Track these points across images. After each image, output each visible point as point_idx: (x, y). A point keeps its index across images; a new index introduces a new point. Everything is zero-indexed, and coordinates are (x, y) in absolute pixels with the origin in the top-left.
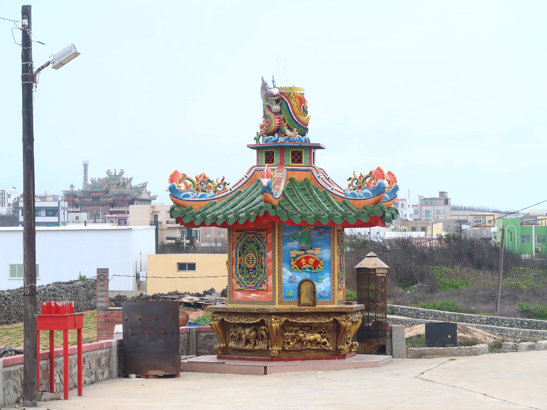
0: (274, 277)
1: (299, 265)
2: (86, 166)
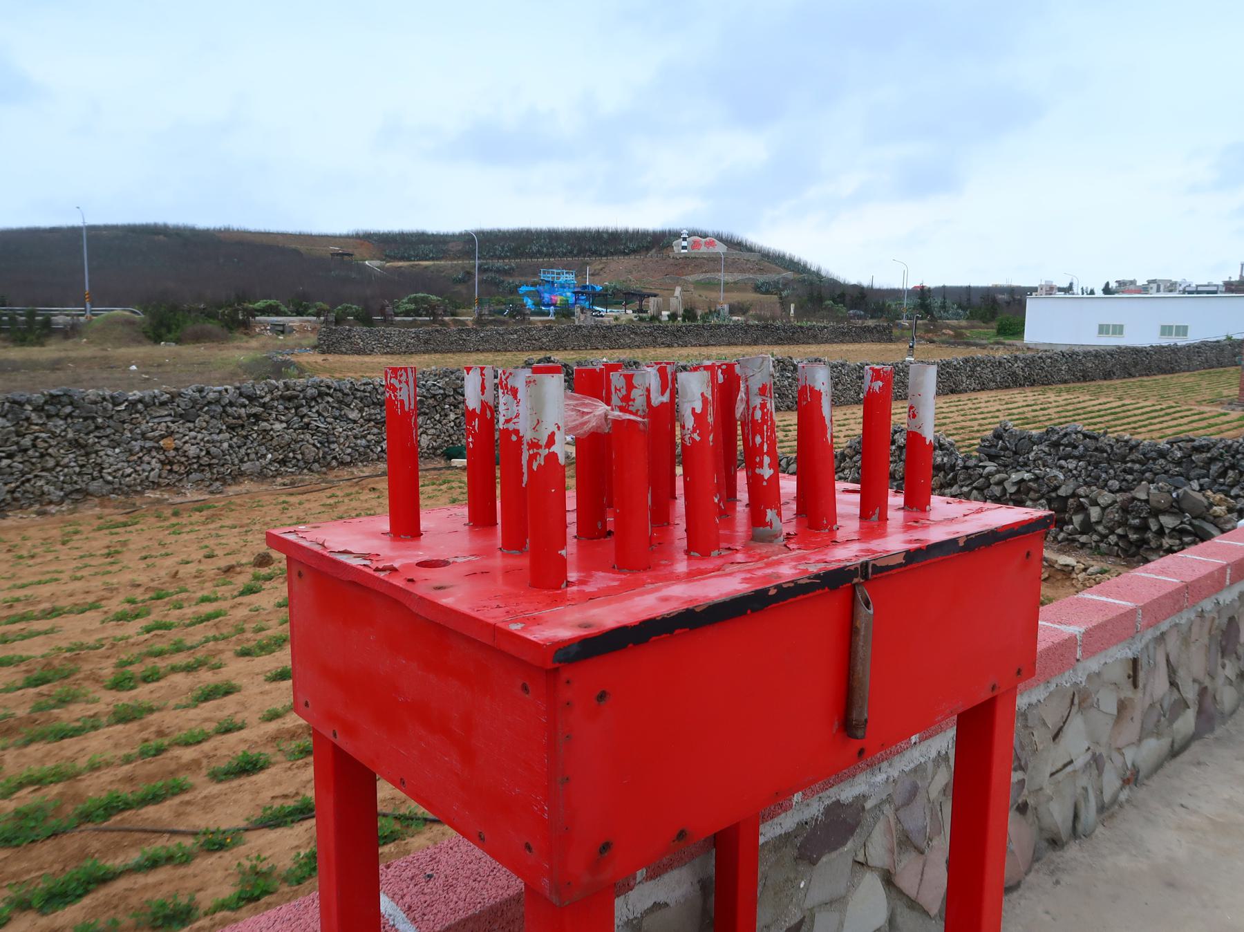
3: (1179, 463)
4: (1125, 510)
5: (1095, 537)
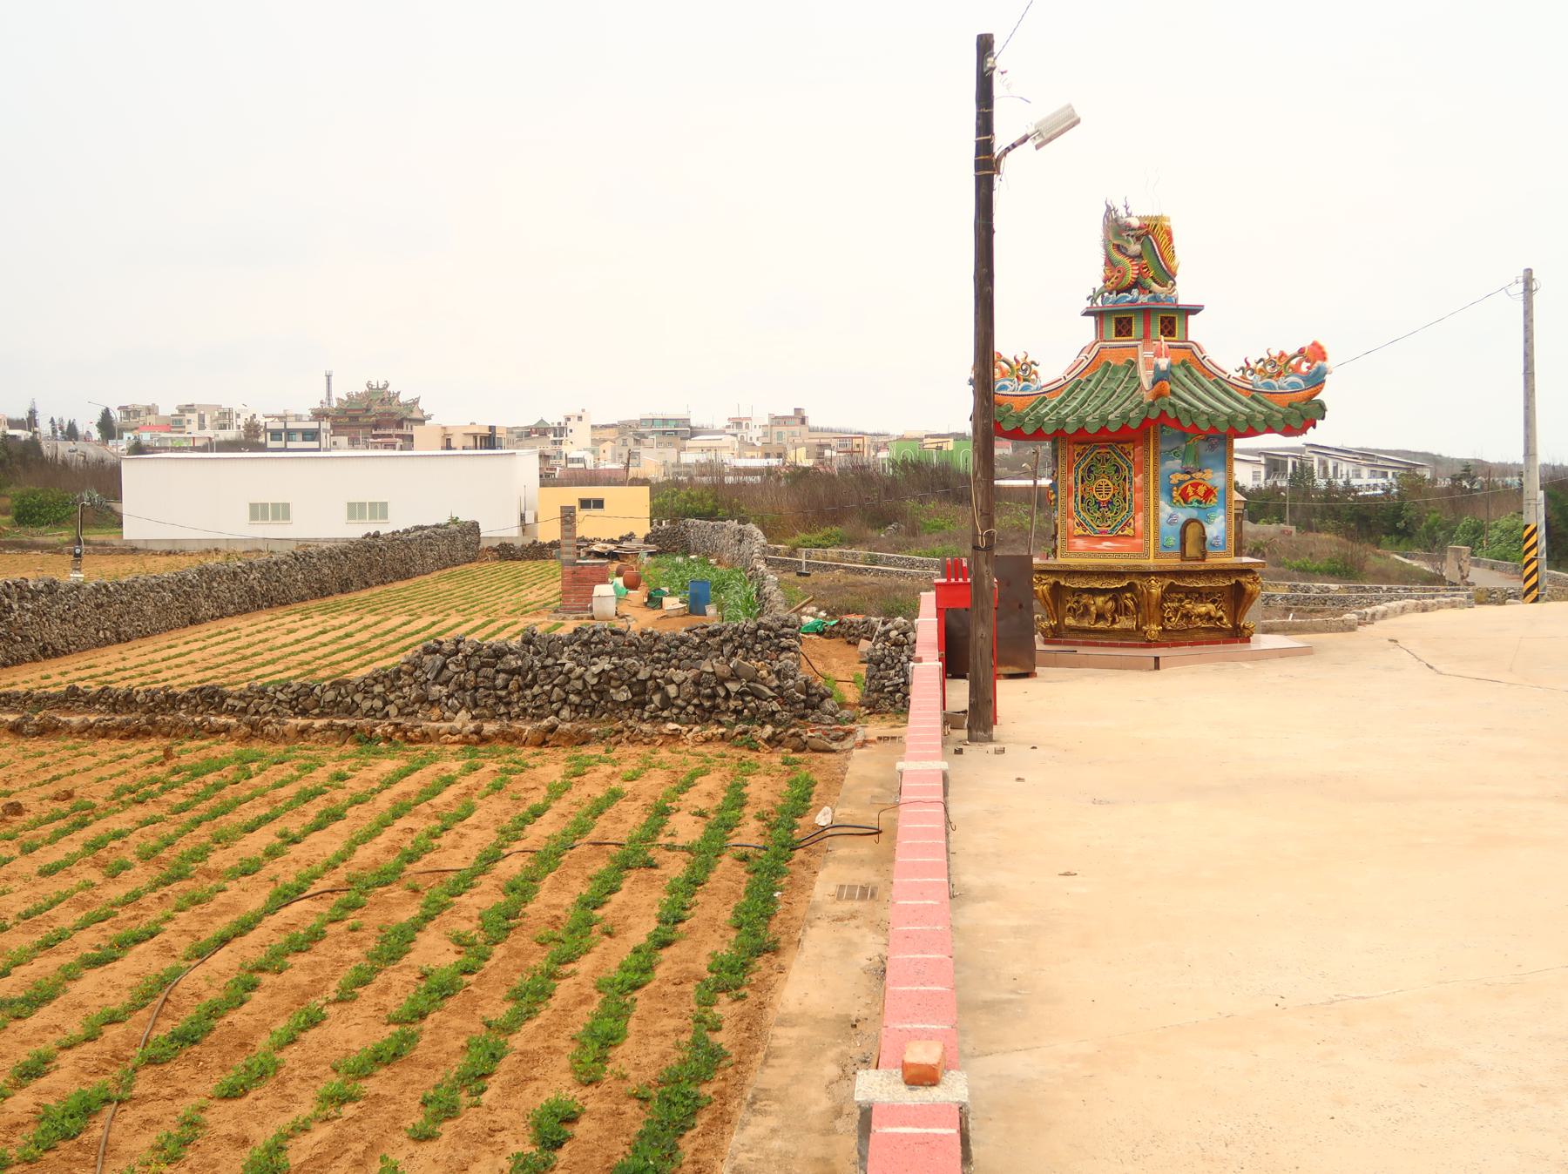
0: (1147, 517)
1: (1185, 497)
2: (329, 377)
3: (697, 648)
4: (697, 683)
5: (675, 711)
